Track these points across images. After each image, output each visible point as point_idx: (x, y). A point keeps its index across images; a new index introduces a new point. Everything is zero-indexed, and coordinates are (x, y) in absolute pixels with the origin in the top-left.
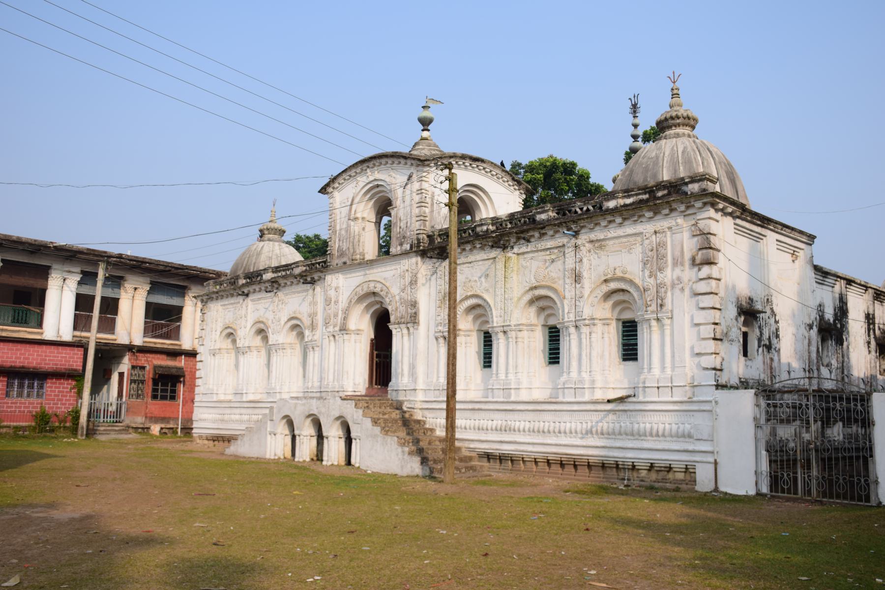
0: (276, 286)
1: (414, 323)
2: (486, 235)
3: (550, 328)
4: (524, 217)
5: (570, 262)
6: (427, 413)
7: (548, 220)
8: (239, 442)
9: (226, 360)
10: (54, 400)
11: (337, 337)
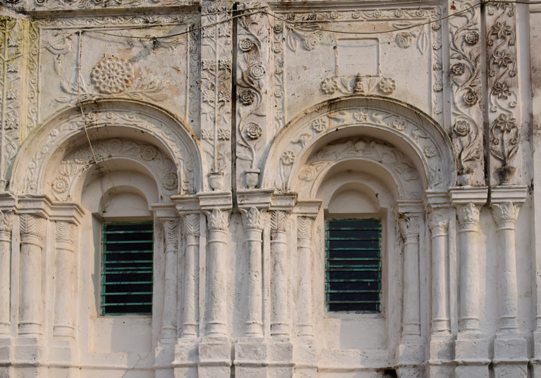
3: (109, 228)
5: (217, 49)
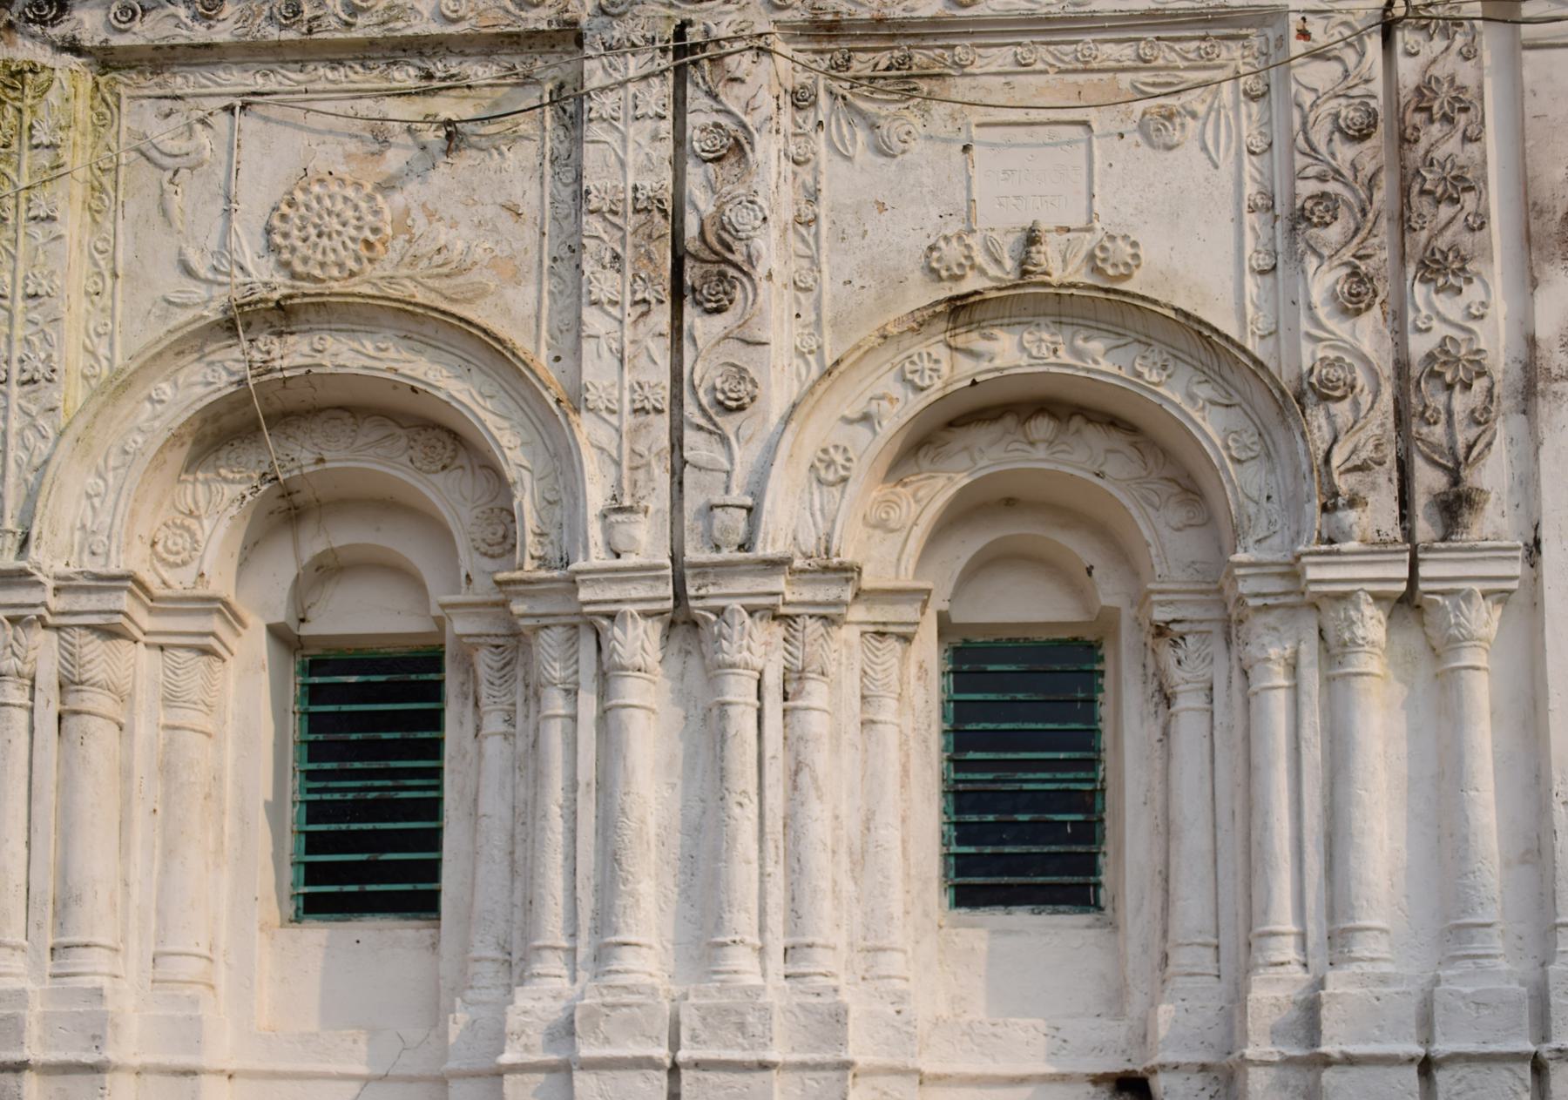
3: (315, 666)
5: (628, 151)
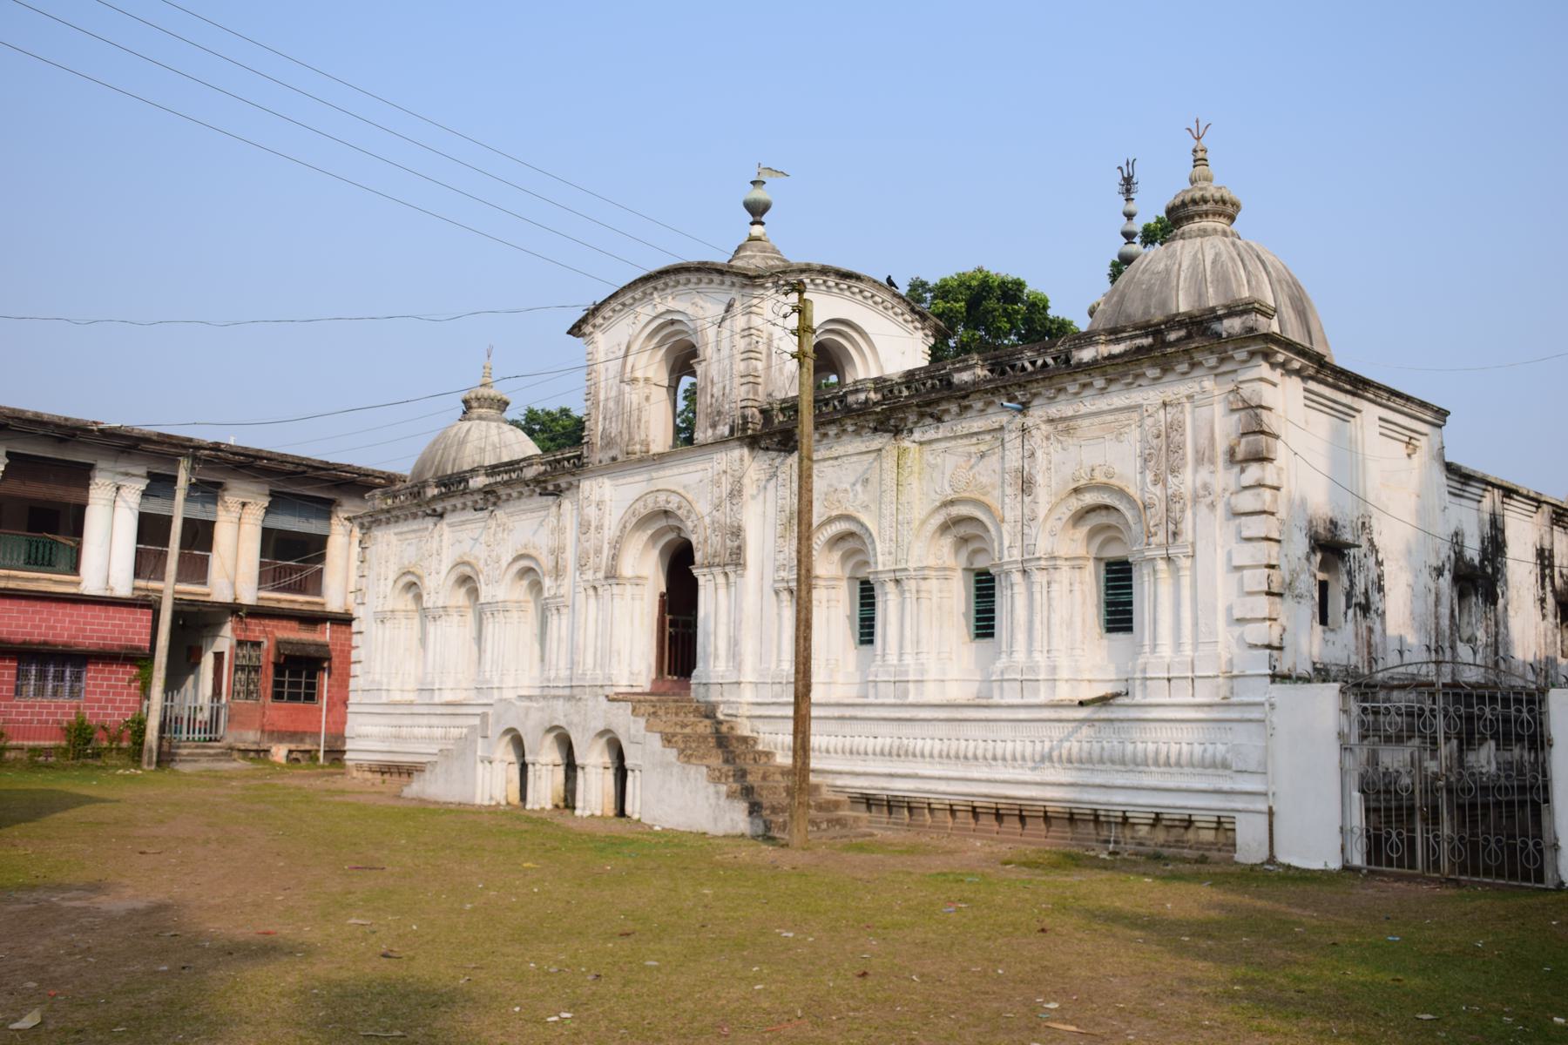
0: (492, 499)
1: (737, 565)
2: (865, 409)
4: (932, 378)
5: (1013, 458)
6: (759, 724)
7: (974, 383)
8: (427, 775)
9: (405, 631)
10: (99, 701)
11: (600, 590)
